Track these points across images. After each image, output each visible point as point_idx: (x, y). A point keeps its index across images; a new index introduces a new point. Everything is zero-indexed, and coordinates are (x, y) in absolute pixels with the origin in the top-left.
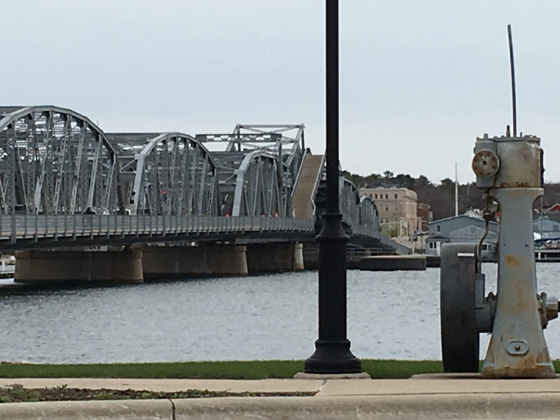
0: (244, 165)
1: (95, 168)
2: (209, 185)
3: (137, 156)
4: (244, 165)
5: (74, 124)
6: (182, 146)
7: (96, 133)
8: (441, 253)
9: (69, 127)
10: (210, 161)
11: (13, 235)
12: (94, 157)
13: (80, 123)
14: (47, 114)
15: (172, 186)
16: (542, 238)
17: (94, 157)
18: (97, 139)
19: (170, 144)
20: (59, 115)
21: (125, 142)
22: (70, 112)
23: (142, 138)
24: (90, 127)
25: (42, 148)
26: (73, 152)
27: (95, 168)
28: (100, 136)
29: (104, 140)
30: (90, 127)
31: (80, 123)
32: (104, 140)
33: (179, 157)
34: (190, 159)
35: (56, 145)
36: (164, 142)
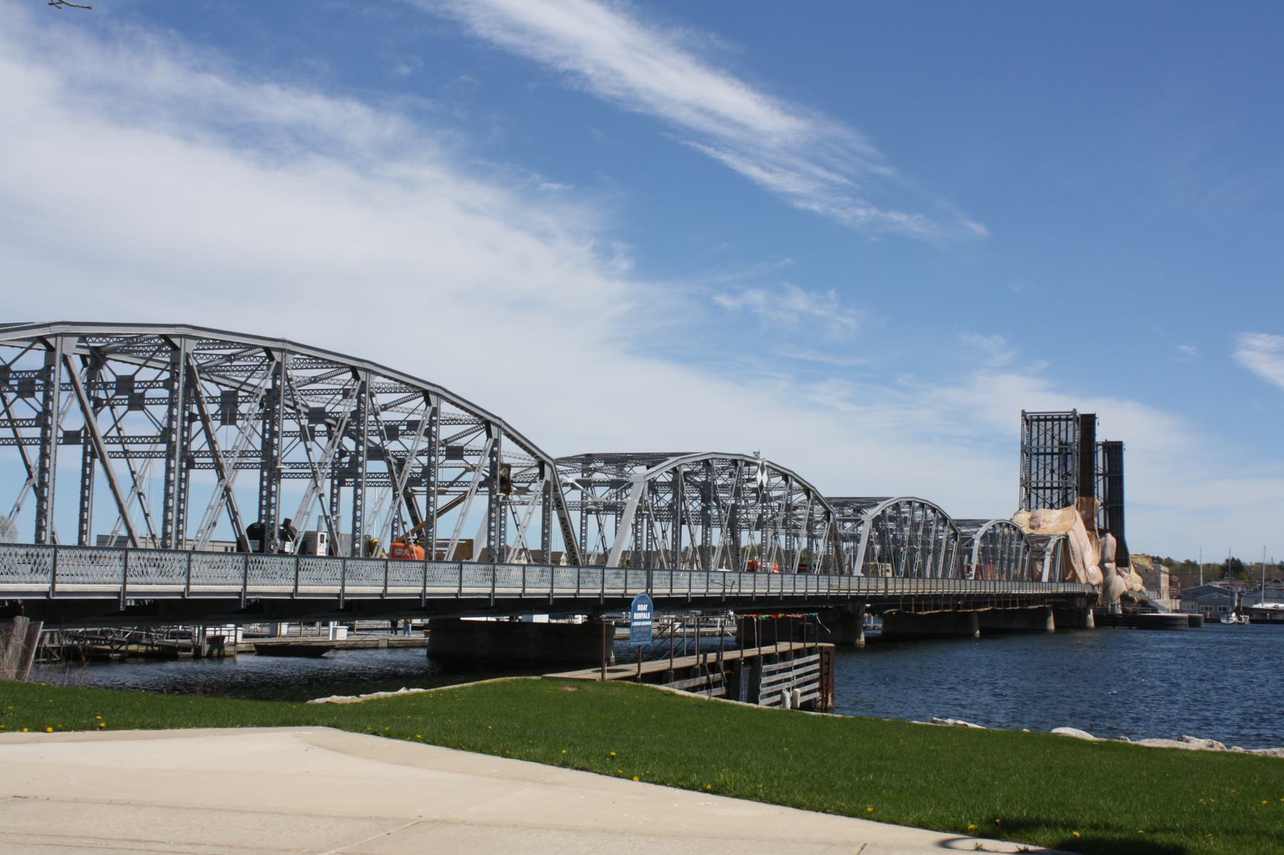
0: (1051, 546)
1: (944, 544)
2: (360, 480)
3: (974, 536)
4: (1051, 546)
5: (929, 511)
6: (1006, 530)
7: (945, 519)
8: (1055, 734)
9: (926, 513)
10: (1026, 542)
11: (886, 592)
12: (942, 537)
13: (934, 510)
14: (910, 503)
15: (1210, 584)
16: (1098, 445)
17: (942, 537)
18: (946, 523)
19: (998, 527)
20: (918, 504)
21: (964, 525)
22: (741, 458)
23: (978, 523)
24: (941, 514)
25: (907, 529)
26: (927, 531)
27: (944, 544)
28: (811, 493)
29: (950, 524)
30: (941, 514)
31: (934, 510)
32: (950, 524)
33: (1004, 537)
34: (1011, 540)
35: (915, 526)
36: (994, 526)
